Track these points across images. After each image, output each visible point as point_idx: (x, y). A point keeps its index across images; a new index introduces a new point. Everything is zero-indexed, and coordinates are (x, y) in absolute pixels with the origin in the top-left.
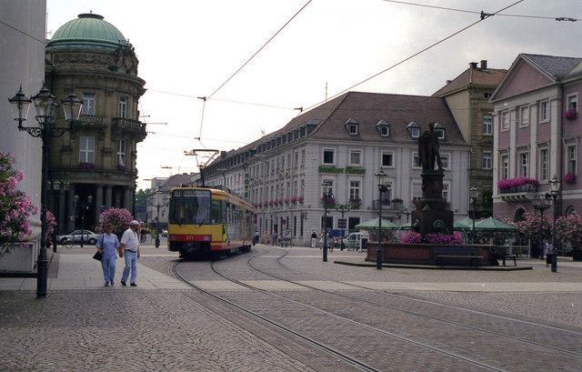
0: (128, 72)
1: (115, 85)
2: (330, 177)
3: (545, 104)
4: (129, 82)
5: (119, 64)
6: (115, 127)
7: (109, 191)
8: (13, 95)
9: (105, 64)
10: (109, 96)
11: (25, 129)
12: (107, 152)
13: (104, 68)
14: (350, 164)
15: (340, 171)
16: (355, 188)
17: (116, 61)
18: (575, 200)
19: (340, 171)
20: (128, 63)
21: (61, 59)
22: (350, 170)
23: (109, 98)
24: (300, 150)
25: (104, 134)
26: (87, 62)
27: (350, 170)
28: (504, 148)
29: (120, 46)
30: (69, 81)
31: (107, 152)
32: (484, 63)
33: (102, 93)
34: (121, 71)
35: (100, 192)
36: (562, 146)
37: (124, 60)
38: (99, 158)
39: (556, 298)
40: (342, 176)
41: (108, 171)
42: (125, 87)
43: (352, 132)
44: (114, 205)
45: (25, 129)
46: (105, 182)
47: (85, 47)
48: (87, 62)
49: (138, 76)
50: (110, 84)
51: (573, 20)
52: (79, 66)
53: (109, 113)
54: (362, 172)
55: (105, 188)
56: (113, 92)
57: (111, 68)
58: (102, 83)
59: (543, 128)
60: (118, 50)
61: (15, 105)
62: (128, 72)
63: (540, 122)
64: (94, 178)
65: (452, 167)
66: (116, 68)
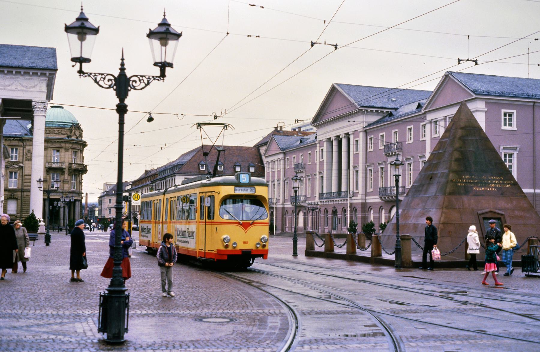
0: (77, 138)
1: (71, 145)
3: (436, 122)
5: (72, 134)
6: (70, 168)
8: (71, 20)
11: (89, 75)
12: (66, 182)
13: (64, 137)
17: (71, 132)
18: (356, 203)
20: (78, 134)
23: (67, 153)
24: (173, 178)
25: (64, 172)
28: (356, 165)
29: (73, 124)
31: (66, 182)
32: (281, 127)
33: (63, 150)
36: (366, 170)
42: (76, 146)
45: (89, 75)
50: (67, 145)
53: (67, 160)
57: (68, 137)
58: (63, 145)
59: (279, 171)
60: (72, 126)
61: (74, 37)
62: (77, 138)
63: (433, 136)
66: (71, 136)
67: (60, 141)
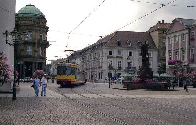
0: (43, 24)
1: (39, 29)
2: (111, 60)
3: (183, 35)
4: (44, 27)
5: (40, 21)
6: (39, 43)
7: (37, 64)
8: (4, 32)
9: (35, 21)
10: (37, 32)
11: (9, 43)
12: (36, 51)
13: (35, 23)
14: (118, 55)
15: (115, 57)
16: (119, 63)
17: (39, 21)
18: (194, 67)
19: (115, 57)
20: (43, 21)
21: (21, 20)
22: (118, 57)
23: (37, 33)
24: (101, 50)
25: (35, 45)
26: (29, 21)
27: (118, 57)
28: (170, 50)
29: (41, 15)
30: (23, 27)
31: (36, 51)
32: (163, 21)
33: (34, 31)
34: (41, 24)
35: (34, 64)
36: (189, 49)
37: (42, 20)
38: (33, 53)
39: (187, 100)
40: (115, 59)
41: (36, 58)
42: (42, 29)
43: (118, 44)
44: (38, 69)
45: (9, 43)
46: (35, 61)
47: (29, 16)
48: (29, 21)
49: (46, 25)
50: (37, 28)
51: (193, 7)
52: (26, 22)
53: (37, 38)
54: (122, 58)
55: (35, 63)
56: (38, 31)
57: (37, 23)
58: (34, 28)
59: (183, 43)
60: (40, 17)
61: (5, 35)
62: (43, 24)
63: (182, 41)
64: (32, 60)
65: (152, 56)
66: (39, 23)
67: (32, 25)
